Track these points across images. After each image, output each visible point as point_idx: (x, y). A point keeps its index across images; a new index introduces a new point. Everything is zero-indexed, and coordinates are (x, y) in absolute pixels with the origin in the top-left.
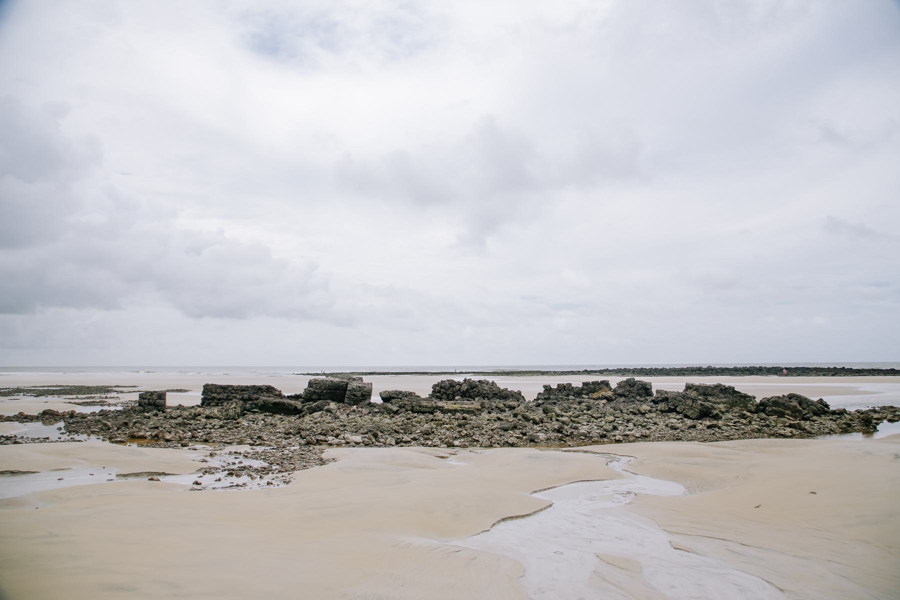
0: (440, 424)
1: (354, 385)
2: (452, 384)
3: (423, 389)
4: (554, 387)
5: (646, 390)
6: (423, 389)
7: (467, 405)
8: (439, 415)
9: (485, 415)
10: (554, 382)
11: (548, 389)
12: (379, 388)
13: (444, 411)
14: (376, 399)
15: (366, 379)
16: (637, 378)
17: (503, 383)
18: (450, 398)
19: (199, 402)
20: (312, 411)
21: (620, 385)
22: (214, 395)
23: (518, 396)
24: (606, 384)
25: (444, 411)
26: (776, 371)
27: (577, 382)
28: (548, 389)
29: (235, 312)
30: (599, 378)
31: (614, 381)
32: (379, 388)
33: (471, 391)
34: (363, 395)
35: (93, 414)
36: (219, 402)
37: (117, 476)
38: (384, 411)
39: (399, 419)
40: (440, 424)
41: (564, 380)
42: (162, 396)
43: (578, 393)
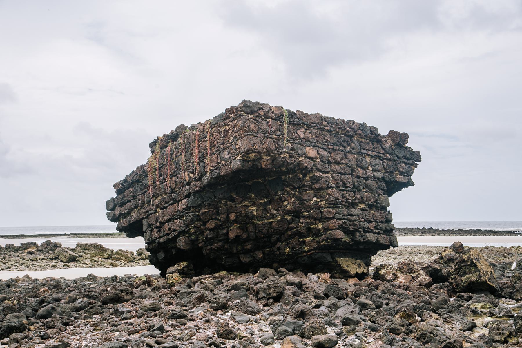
24: (35, 244)
27: (17, 242)
31: (40, 242)
43: (17, 250)
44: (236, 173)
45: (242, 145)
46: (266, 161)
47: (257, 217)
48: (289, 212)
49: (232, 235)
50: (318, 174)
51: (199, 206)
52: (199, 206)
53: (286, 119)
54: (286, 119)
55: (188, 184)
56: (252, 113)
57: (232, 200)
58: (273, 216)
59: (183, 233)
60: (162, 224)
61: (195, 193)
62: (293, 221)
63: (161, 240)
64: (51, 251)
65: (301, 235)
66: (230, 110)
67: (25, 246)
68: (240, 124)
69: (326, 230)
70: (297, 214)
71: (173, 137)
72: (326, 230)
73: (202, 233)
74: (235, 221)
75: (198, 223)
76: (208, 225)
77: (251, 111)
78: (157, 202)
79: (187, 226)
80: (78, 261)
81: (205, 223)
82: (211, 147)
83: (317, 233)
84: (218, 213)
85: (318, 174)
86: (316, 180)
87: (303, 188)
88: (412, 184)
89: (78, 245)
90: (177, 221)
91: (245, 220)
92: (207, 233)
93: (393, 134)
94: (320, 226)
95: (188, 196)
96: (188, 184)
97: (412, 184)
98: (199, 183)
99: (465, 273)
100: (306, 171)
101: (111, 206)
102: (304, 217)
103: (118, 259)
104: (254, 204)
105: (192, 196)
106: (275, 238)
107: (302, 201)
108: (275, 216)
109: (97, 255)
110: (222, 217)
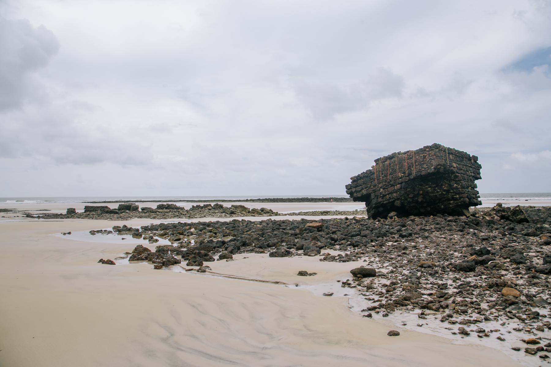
0: (158, 215)
1: (134, 205)
2: (163, 205)
3: (154, 206)
4: (195, 206)
5: (221, 207)
6: (154, 206)
7: (166, 210)
8: (158, 213)
9: (171, 213)
10: (195, 204)
11: (193, 206)
12: (141, 206)
13: (159, 212)
14: (140, 210)
15: (137, 204)
16: (219, 203)
17: (178, 204)
18: (162, 209)
19: (84, 211)
20: (122, 213)
21: (214, 205)
22: (87, 209)
23: (182, 209)
24: (210, 205)
25: (159, 212)
26: (259, 200)
27: (202, 204)
28: (193, 206)
29: (93, 160)
30: (208, 203)
31: (213, 204)
32: (141, 206)
33: (168, 207)
34: (136, 208)
35: (261, 223)
36: (91, 211)
37: (514, 329)
38: (142, 212)
39: (147, 214)
40: (158, 215)
41: (198, 204)
42: (74, 209)
43: (202, 208)
44: (429, 174)
45: (434, 163)
46: (442, 170)
47: (431, 193)
48: (445, 190)
49: (420, 200)
50: (457, 174)
51: (407, 188)
52: (407, 188)
53: (447, 151)
54: (447, 151)
55: (401, 178)
56: (437, 148)
57: (421, 185)
58: (438, 192)
59: (398, 199)
60: (384, 196)
61: (405, 182)
62: (446, 194)
63: (385, 202)
64: (218, 208)
65: (449, 200)
66: (426, 147)
67: (205, 206)
68: (433, 153)
69: (460, 198)
70: (448, 191)
71: (390, 157)
72: (460, 198)
73: (406, 199)
74: (421, 194)
75: (406, 195)
76: (410, 196)
77: (436, 149)
78: (380, 186)
79: (401, 196)
80: (235, 214)
81: (408, 196)
82: (415, 163)
83: (455, 199)
84: (414, 191)
85: (457, 174)
86: (457, 177)
87: (450, 180)
88: (480, 178)
89: (232, 206)
90: (395, 194)
91: (426, 194)
92: (409, 199)
93: (473, 156)
94: (458, 196)
95: (401, 183)
96: (401, 178)
97: (480, 178)
98: (408, 178)
99: (518, 215)
100: (453, 172)
101: (349, 187)
102: (451, 193)
103: (254, 213)
104: (430, 187)
105: (403, 184)
106: (438, 201)
107: (450, 186)
108: (439, 192)
109: (242, 211)
110: (416, 193)
